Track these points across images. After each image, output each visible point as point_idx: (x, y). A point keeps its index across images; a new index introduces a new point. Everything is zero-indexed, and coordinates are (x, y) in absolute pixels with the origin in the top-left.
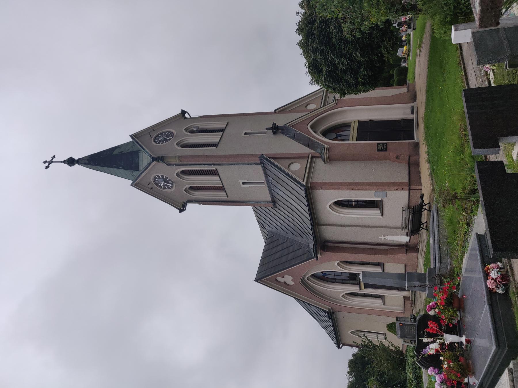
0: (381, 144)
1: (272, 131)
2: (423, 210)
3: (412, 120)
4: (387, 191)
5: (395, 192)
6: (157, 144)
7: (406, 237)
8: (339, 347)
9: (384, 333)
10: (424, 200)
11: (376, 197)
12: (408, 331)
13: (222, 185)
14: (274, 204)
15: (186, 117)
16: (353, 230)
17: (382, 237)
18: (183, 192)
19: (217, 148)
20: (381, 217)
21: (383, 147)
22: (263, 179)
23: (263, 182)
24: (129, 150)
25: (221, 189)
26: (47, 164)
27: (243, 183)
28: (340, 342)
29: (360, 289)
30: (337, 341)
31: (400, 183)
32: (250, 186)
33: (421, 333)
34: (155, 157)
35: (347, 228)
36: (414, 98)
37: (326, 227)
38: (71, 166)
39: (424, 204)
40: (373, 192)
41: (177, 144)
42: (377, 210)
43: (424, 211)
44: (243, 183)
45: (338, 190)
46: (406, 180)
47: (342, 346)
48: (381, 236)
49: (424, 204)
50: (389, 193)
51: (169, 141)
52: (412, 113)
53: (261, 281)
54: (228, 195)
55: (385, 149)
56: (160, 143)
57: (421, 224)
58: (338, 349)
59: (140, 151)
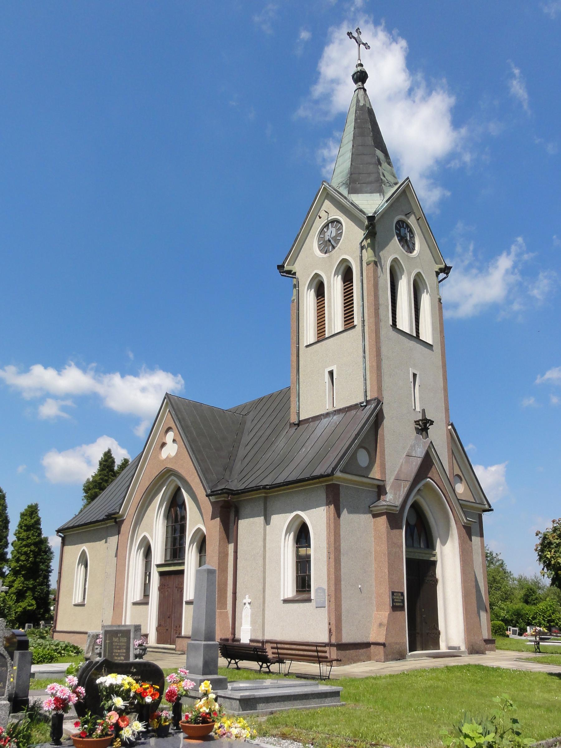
0: (402, 598)
1: (420, 420)
2: (260, 663)
3: (436, 645)
4: (326, 607)
5: (326, 621)
6: (396, 226)
7: (250, 639)
8: (58, 531)
9: (85, 603)
10: (274, 664)
11: (316, 590)
12: (116, 644)
13: (327, 336)
14: (295, 425)
15: (439, 274)
16: (258, 553)
17: (247, 600)
18: (313, 271)
19: (390, 326)
20: (282, 598)
21: (397, 600)
22: (338, 406)
23: (334, 406)
24: (384, 177)
25: (321, 336)
26: (355, 34)
27: (331, 373)
28: (66, 532)
29: (158, 566)
30: (68, 528)
31: (341, 630)
32: (327, 383)
33: (133, 669)
34: (375, 222)
35: (261, 543)
36: (473, 650)
37: (263, 510)
38: (367, 77)
39: (238, 662)
40: (325, 586)
41: (396, 258)
42: (293, 591)
43: (259, 664)
44: (331, 373)
45: (327, 529)
46: (346, 638)
47: (60, 536)
48: (249, 598)
49: (269, 664)
50: (324, 613)
51: (341, 240)
52: (450, 648)
53: (167, 403)
54: (310, 348)
55: (394, 604)
56: (397, 230)
57: (235, 661)
58: (56, 531)
59: (382, 196)
